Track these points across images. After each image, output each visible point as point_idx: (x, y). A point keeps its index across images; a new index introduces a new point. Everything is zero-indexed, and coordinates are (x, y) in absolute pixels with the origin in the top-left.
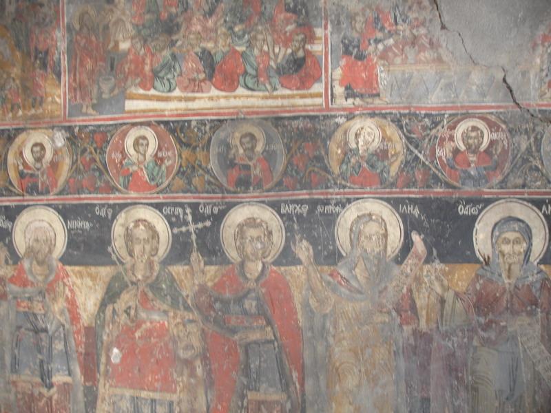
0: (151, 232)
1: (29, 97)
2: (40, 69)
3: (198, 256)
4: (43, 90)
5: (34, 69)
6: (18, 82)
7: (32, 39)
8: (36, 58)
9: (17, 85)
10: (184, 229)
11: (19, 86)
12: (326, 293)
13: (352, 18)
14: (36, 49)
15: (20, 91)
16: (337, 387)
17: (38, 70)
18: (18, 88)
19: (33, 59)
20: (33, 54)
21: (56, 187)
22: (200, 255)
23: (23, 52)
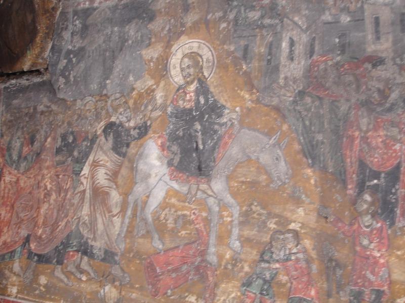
0: (187, 192)
1: (340, 287)
2: (374, 215)
3: (102, 127)
4: (383, 272)
5: (356, 216)
6: (307, 243)
7: (352, 139)
8: (361, 187)
9: (305, 251)
10: (246, 233)
11: (314, 254)
12: (89, 128)
13: (57, 172)
14: (362, 165)
15: (315, 267)
16: (69, 103)
17: (367, 219)
18: (309, 261)
19: (351, 190)
20: (353, 178)
21: (41, 37)
22: (103, 128)
23: (324, 169)
